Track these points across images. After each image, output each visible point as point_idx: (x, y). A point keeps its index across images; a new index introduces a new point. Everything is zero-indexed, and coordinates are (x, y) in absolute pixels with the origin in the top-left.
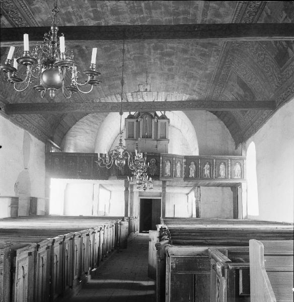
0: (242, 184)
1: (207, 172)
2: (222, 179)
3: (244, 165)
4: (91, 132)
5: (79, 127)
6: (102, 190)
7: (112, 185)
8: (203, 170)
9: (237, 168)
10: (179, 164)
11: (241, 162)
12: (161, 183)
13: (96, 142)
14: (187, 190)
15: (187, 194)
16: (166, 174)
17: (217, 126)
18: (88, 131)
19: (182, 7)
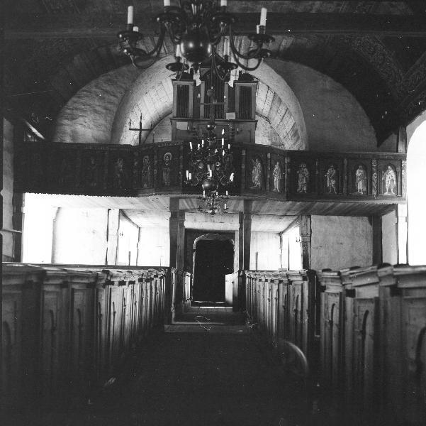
0: (399, 206)
1: (331, 183)
2: (360, 197)
3: (403, 171)
4: (104, 111)
5: (82, 101)
6: (124, 223)
7: (143, 212)
8: (324, 180)
9: (390, 175)
10: (277, 167)
11: (396, 163)
12: (241, 207)
13: (116, 127)
14: (281, 225)
15: (280, 234)
16: (254, 184)
17: (345, 103)
18: (98, 108)
19: (249, 4)
